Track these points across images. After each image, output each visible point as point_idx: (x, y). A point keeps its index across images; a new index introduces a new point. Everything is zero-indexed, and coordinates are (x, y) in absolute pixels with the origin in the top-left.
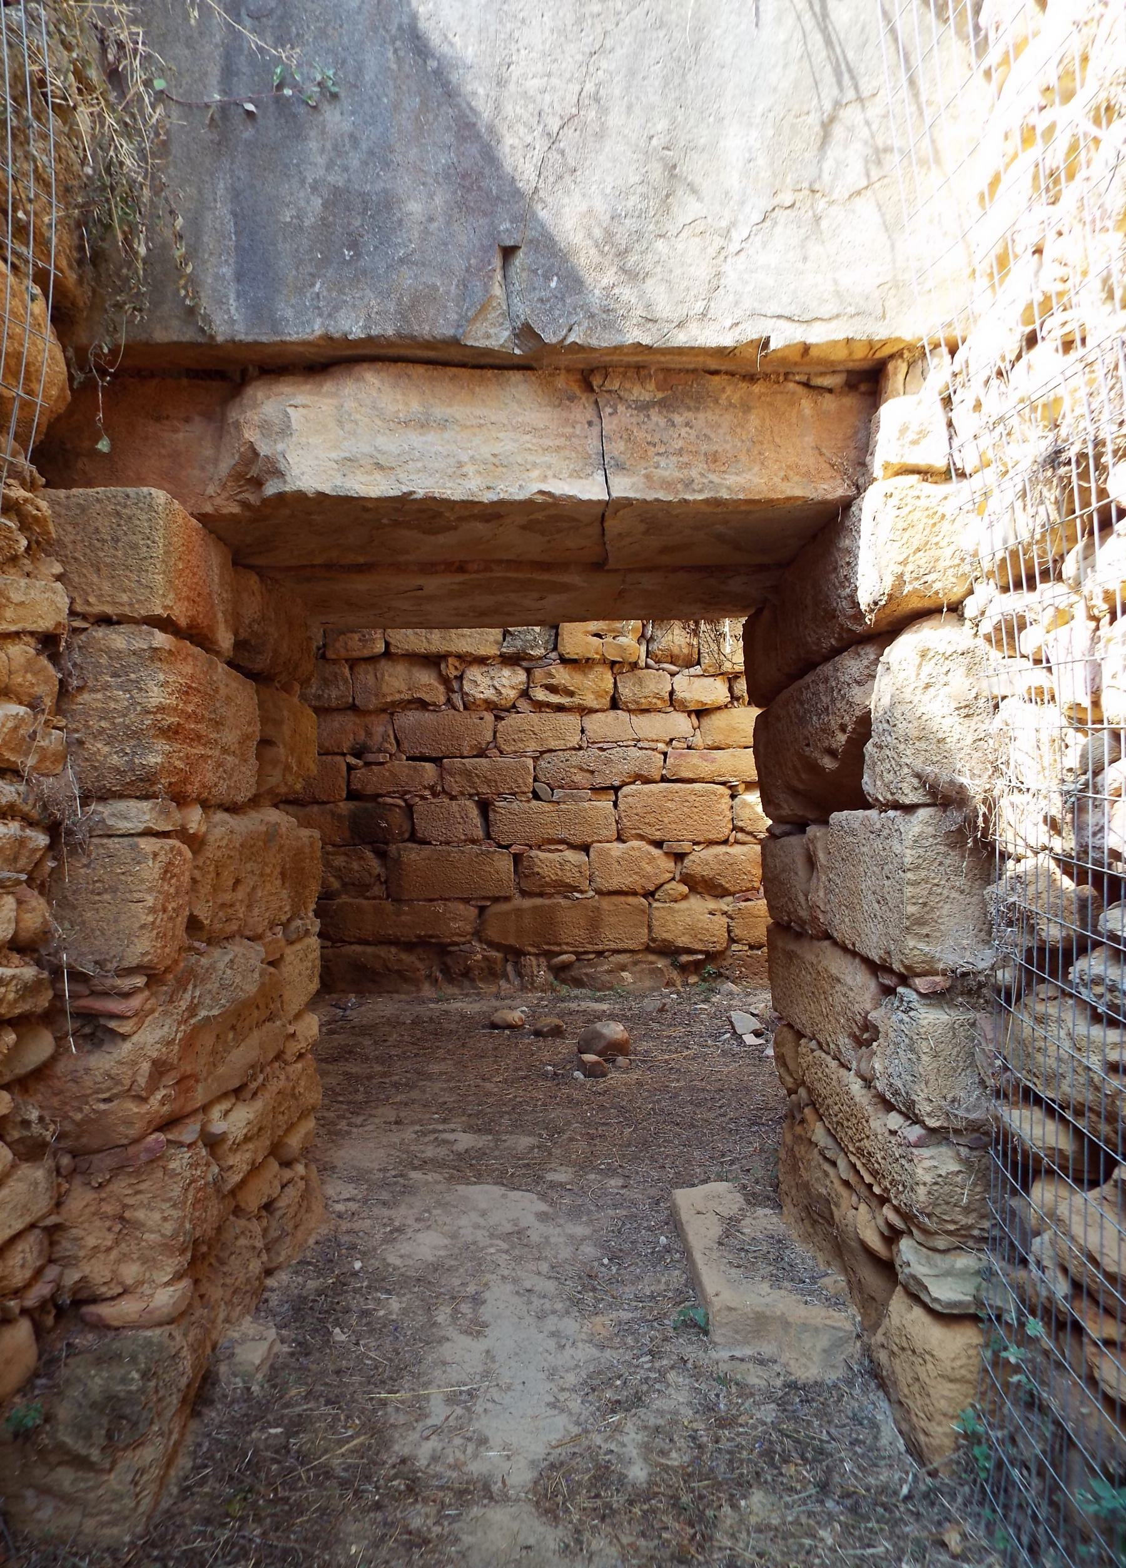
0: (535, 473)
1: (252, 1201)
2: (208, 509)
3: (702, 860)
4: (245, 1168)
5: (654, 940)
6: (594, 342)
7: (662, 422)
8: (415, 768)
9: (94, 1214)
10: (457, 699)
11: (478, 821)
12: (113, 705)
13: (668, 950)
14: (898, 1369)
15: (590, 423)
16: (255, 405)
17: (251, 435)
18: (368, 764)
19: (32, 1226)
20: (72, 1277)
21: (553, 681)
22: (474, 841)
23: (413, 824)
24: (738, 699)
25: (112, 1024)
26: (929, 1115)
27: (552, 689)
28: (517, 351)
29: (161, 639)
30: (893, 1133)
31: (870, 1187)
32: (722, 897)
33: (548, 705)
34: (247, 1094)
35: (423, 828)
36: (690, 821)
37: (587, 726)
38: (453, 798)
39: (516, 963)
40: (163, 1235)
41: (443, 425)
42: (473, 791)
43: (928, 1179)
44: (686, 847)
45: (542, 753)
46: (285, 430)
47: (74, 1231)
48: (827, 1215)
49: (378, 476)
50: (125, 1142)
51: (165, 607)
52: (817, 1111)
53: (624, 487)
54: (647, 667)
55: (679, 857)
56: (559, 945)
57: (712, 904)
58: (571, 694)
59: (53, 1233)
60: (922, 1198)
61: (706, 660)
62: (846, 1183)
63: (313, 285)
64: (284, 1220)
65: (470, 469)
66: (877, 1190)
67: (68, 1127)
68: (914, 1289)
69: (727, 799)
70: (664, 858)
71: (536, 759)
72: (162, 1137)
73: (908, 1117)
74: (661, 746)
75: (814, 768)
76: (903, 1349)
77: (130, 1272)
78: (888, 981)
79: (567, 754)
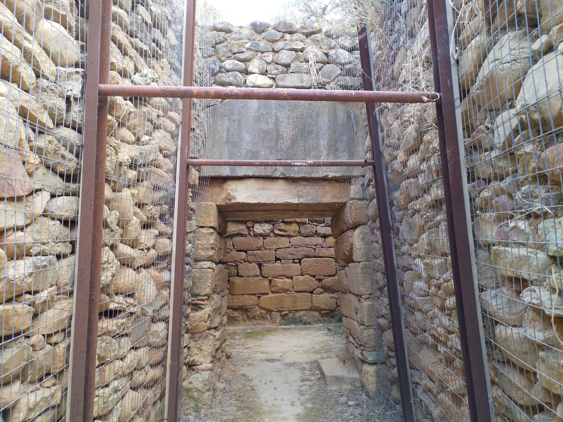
2: (218, 204)
10: (252, 233)
11: (258, 270)
16: (230, 186)
17: (229, 191)
20: (192, 359)
21: (281, 228)
22: (256, 276)
27: (279, 230)
35: (241, 272)
38: (250, 263)
44: (322, 277)
46: (236, 190)
49: (254, 199)
53: (302, 201)
54: (309, 223)
55: (320, 280)
57: (331, 295)
58: (286, 231)
62: (356, 347)
65: (272, 197)
67: (192, 327)
71: (275, 251)
74: (313, 247)
75: (345, 254)
77: (202, 360)
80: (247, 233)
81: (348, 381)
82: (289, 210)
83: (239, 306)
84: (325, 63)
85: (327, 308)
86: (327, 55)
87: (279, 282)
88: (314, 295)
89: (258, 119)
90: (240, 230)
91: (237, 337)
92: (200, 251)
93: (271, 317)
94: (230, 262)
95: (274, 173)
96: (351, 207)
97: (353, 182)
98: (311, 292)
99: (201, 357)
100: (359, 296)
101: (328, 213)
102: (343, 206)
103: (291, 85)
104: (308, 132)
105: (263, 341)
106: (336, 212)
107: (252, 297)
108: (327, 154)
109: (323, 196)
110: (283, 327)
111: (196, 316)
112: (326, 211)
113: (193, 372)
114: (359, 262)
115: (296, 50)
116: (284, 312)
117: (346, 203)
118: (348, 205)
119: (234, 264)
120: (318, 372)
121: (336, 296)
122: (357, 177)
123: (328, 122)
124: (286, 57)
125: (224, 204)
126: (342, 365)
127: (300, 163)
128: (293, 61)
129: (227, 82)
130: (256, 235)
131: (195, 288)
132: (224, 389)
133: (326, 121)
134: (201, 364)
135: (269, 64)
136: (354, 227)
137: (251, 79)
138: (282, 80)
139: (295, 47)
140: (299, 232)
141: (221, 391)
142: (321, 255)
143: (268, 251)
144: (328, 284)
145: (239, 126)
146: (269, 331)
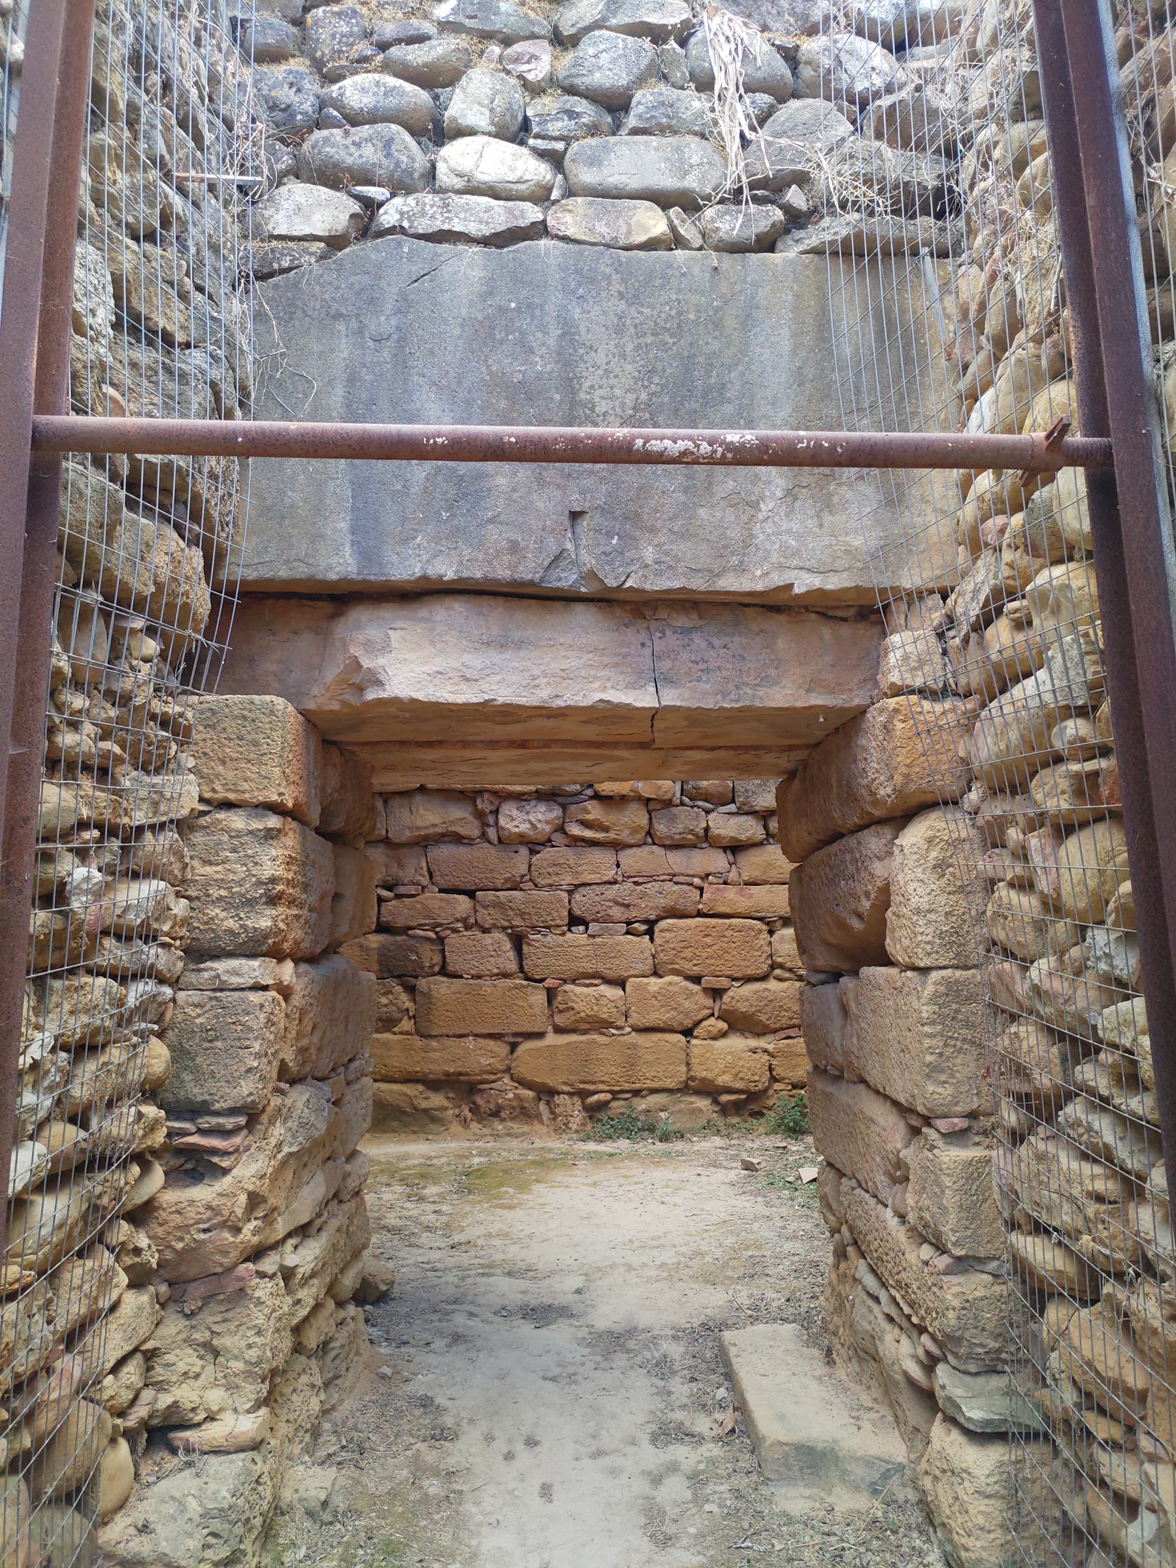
0: (596, 685)
1: (312, 1339)
2: (311, 705)
3: (741, 996)
4: (312, 1302)
5: (693, 1078)
6: (648, 587)
7: (704, 645)
8: (448, 902)
9: (185, 1341)
10: (492, 833)
11: (511, 954)
12: (231, 876)
13: (709, 1090)
14: (941, 1492)
15: (643, 645)
16: (358, 627)
17: (354, 650)
18: (398, 897)
19: (136, 1350)
20: (165, 1400)
21: (589, 817)
22: (506, 975)
23: (444, 957)
24: (773, 837)
25: (215, 1160)
26: (954, 1244)
28: (583, 590)
29: (273, 821)
30: (926, 1263)
31: (909, 1317)
32: (764, 1034)
33: (583, 839)
34: (313, 1230)
35: (455, 962)
36: (727, 956)
37: (622, 862)
38: (485, 931)
39: (548, 1103)
40: (246, 1362)
41: (520, 645)
42: (506, 924)
43: (956, 1303)
44: (724, 982)
45: (577, 886)
47: (166, 1357)
48: (872, 1351)
49: (464, 686)
50: (219, 1270)
51: (280, 794)
52: (859, 1248)
53: (671, 697)
54: (682, 804)
56: (594, 1083)
57: (753, 1043)
59: (150, 1356)
60: (953, 1322)
61: (740, 800)
63: (415, 538)
64: (337, 1362)
65: (542, 681)
66: (915, 1320)
67: (169, 1255)
68: (951, 1411)
69: (765, 935)
70: (701, 994)
71: (570, 893)
72: (250, 1265)
73: (938, 1248)
74: (697, 881)
75: (843, 926)
76: (944, 1471)
77: (215, 1397)
78: (915, 1122)
79: (603, 888)
80: (476, 833)
81: (859, 1472)
82: (615, 745)
83: (447, 1074)
84: (783, 94)
85: (739, 1085)
86: (791, 56)
87: (583, 997)
88: (694, 1042)
89: (486, 332)
90: (452, 823)
91: (432, 1190)
92: (215, 912)
93: (552, 1112)
94: (420, 927)
95: (555, 573)
96: (887, 728)
97: (898, 618)
98: (688, 1033)
99: (215, 1384)
100: (919, 1123)
101: (769, 758)
102: (849, 723)
103: (634, 184)
104: (705, 394)
105: (518, 1213)
106: (801, 755)
107: (491, 1044)
108: (789, 492)
109: (765, 680)
110: (592, 1146)
111: (192, 1202)
112: (768, 749)
113: (172, 1462)
114: (925, 971)
115: (658, 35)
116: (596, 1097)
117: (862, 711)
118: (875, 718)
119: (431, 935)
120: (721, 1393)
121: (770, 1047)
122: (916, 597)
123: (794, 352)
124: (614, 61)
125: (336, 706)
126: (821, 1369)
127: (682, 445)
128: (641, 81)
129: (349, 170)
130: (505, 841)
131: (187, 1077)
132: (325, 1504)
133: (786, 346)
134: (211, 1418)
135: (534, 90)
136: (903, 816)
137: (456, 157)
138: (594, 161)
139: (654, 19)
140: (649, 833)
141: (310, 1514)
142: (722, 909)
143: (543, 894)
144: (743, 1007)
145: (402, 362)
146: (544, 1164)
